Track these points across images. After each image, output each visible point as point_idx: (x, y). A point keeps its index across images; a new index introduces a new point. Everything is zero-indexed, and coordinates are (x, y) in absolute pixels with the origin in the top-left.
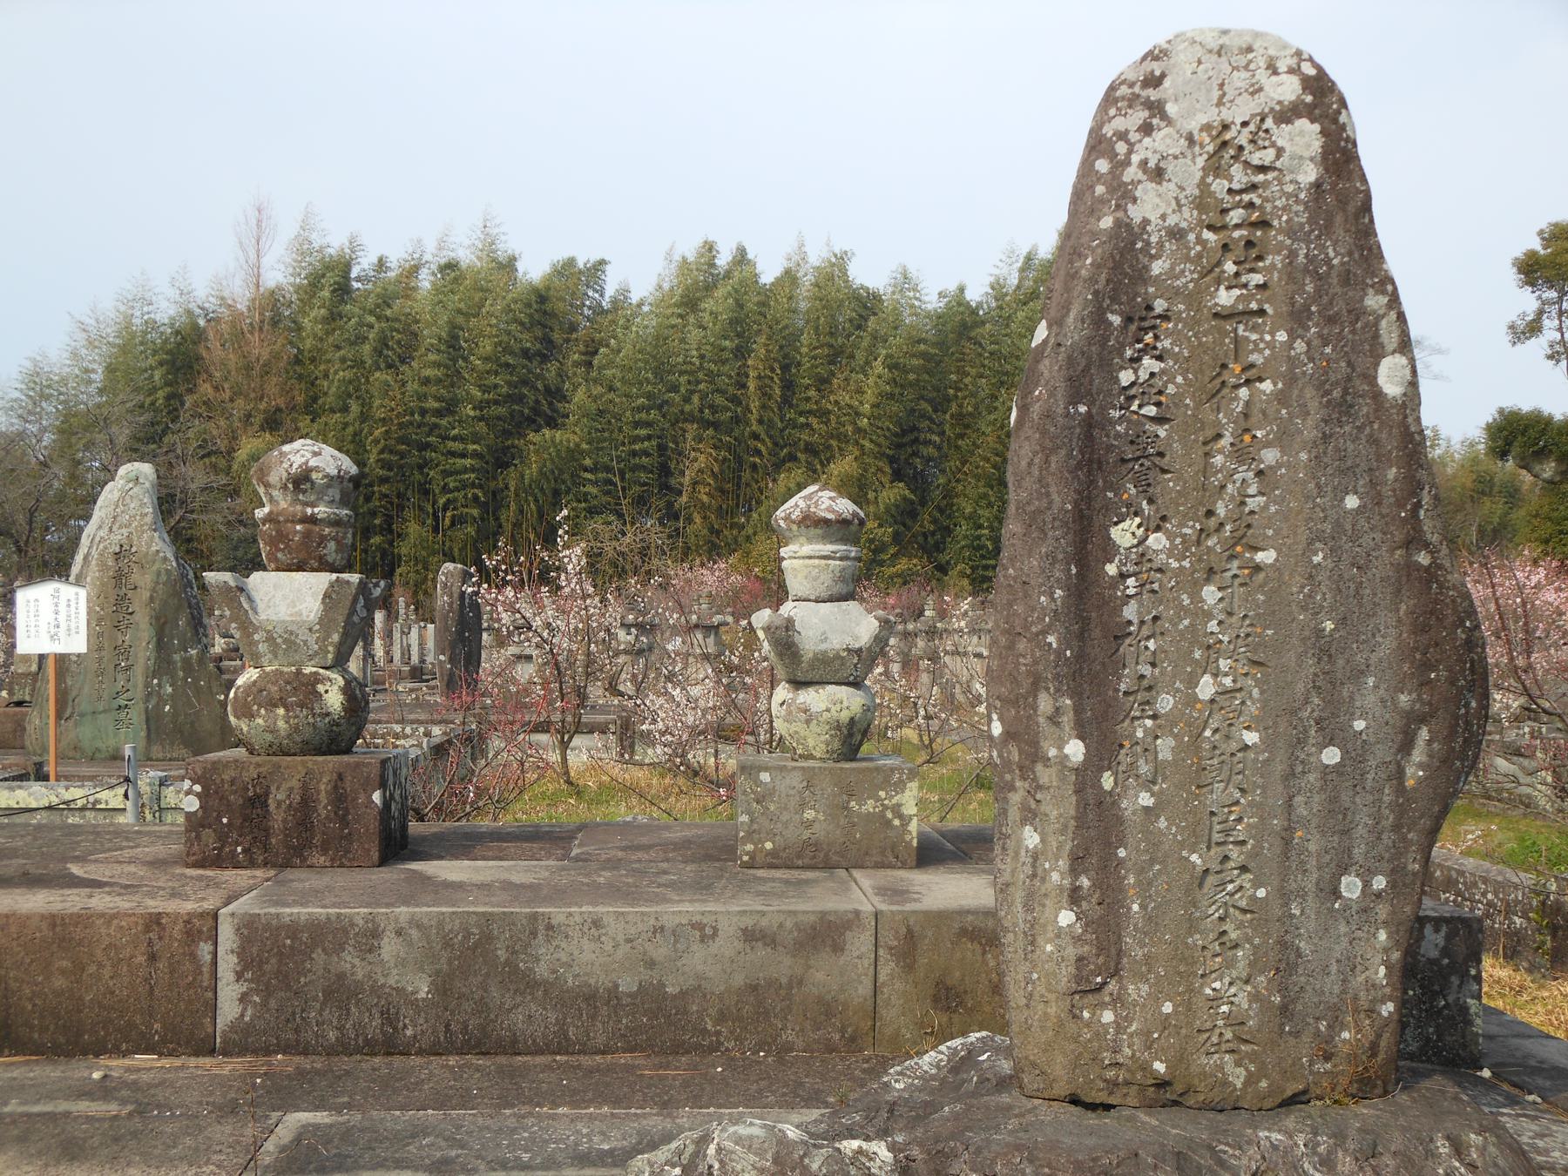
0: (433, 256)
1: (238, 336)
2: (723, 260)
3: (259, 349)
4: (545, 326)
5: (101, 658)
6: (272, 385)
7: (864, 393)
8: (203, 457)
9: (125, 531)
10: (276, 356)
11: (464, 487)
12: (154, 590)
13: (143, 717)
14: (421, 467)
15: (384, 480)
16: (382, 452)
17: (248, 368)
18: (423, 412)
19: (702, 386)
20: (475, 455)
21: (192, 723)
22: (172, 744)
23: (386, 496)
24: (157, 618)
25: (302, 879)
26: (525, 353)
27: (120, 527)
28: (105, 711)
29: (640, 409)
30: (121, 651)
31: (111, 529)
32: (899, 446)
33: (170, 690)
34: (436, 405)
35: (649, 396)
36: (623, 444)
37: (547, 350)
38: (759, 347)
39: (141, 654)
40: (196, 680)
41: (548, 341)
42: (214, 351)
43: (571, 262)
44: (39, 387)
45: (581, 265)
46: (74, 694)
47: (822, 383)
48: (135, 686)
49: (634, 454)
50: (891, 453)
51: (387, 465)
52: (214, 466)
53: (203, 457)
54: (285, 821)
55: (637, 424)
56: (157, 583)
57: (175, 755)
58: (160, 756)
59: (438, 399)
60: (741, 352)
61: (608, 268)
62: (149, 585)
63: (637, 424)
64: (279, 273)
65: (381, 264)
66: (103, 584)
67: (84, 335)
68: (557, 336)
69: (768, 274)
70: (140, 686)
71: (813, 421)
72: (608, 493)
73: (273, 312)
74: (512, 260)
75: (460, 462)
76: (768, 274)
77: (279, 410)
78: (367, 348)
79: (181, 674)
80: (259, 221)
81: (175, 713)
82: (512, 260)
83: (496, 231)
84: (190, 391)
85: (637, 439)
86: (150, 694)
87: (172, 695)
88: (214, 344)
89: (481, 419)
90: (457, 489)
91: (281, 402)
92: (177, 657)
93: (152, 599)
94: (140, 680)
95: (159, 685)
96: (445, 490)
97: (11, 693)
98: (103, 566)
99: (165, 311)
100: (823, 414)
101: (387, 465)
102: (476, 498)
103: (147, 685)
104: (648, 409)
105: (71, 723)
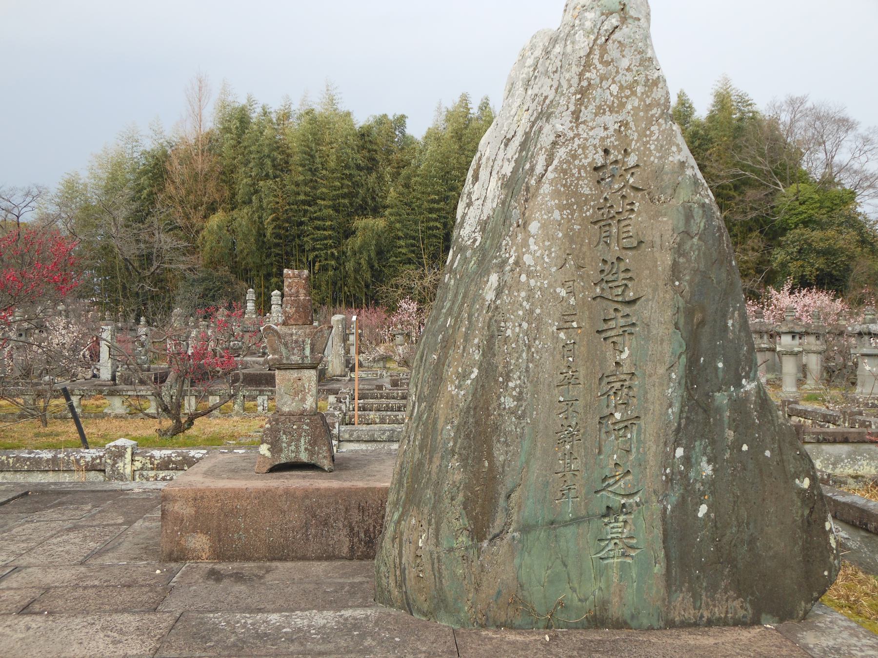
0: (297, 107)
1: (187, 159)
2: (475, 111)
3: (201, 165)
5: (570, 402)
6: (211, 185)
8: (170, 230)
9: (610, 119)
10: (212, 170)
11: (326, 248)
12: (679, 250)
13: (658, 532)
14: (299, 236)
15: (277, 245)
16: (275, 228)
17: (195, 177)
20: (331, 228)
21: (752, 541)
22: (713, 588)
23: (278, 254)
24: (689, 313)
25: (245, 487)
26: (359, 168)
27: (600, 111)
28: (577, 521)
29: (433, 201)
30: (612, 383)
31: (576, 115)
33: (707, 470)
35: (438, 193)
36: (423, 222)
39: (654, 394)
40: (757, 448)
42: (176, 167)
43: (385, 116)
44: (71, 190)
46: (509, 482)
48: (641, 463)
49: (430, 228)
51: (278, 236)
52: (176, 235)
53: (170, 230)
55: (431, 211)
56: (687, 234)
57: (719, 612)
58: (690, 614)
59: (306, 194)
62: (670, 239)
63: (431, 211)
64: (210, 122)
66: (571, 238)
70: (652, 461)
72: (413, 252)
73: (210, 144)
74: (348, 114)
77: (215, 201)
79: (730, 434)
80: (200, 89)
81: (717, 523)
82: (348, 114)
84: (161, 190)
85: (429, 220)
86: (670, 480)
87: (712, 484)
88: (176, 162)
90: (321, 249)
91: (217, 196)
92: (721, 398)
93: (675, 271)
94: (652, 449)
95: (687, 460)
96: (314, 249)
97: (275, 448)
98: (570, 197)
99: (149, 145)
101: (278, 236)
102: (333, 254)
103: (667, 459)
104: (438, 202)
105: (502, 547)
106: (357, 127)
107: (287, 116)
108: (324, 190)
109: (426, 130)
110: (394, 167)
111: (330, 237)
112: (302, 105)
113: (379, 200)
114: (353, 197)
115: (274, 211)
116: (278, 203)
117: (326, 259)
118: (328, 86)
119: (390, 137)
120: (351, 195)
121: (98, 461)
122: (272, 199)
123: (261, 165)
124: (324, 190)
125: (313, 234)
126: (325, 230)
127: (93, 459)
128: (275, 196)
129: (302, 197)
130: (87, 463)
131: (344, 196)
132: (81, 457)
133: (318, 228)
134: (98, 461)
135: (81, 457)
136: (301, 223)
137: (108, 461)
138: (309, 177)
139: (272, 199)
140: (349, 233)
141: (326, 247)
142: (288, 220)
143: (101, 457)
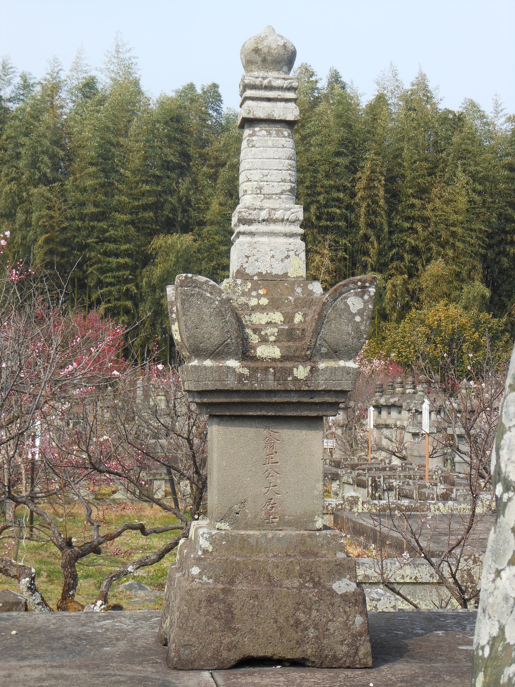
0: (71, 79)
2: (323, 84)
4: (182, 143)
7: (454, 198)
18: (82, 218)
19: (321, 198)
20: (128, 254)
32: (490, 247)
34: (93, 210)
37: (182, 166)
38: (369, 160)
41: (185, 156)
43: (191, 87)
45: (199, 91)
47: (423, 192)
50: (483, 251)
54: (25, 578)
60: (353, 168)
61: (345, 78)
65: (26, 86)
67: (343, 132)
68: (192, 151)
69: (365, 95)
71: (418, 226)
75: (114, 260)
76: (365, 95)
78: (21, 164)
83: (127, 55)
89: (132, 223)
90: (111, 284)
96: (100, 284)
100: (425, 220)
106: (153, 106)
107: (53, 88)
108: (124, 198)
109: (180, 84)
110: (211, 166)
111: (125, 266)
112: (75, 69)
113: (193, 214)
114: (157, 208)
115: (45, 230)
116: (52, 217)
117: (118, 299)
118: (117, 46)
119: (204, 117)
120: (156, 207)
121: (340, 507)
122: (45, 212)
123: (34, 164)
124: (124, 198)
125: (99, 262)
126: (117, 256)
127: (337, 506)
128: (49, 208)
129: (90, 209)
130: (333, 508)
131: (145, 208)
132: (329, 504)
133: (106, 254)
134: (340, 507)
135: (329, 504)
136: (83, 247)
137: (348, 507)
138: (103, 180)
139: (45, 212)
140: (147, 260)
141: (120, 281)
142: (64, 243)
143: (342, 504)
